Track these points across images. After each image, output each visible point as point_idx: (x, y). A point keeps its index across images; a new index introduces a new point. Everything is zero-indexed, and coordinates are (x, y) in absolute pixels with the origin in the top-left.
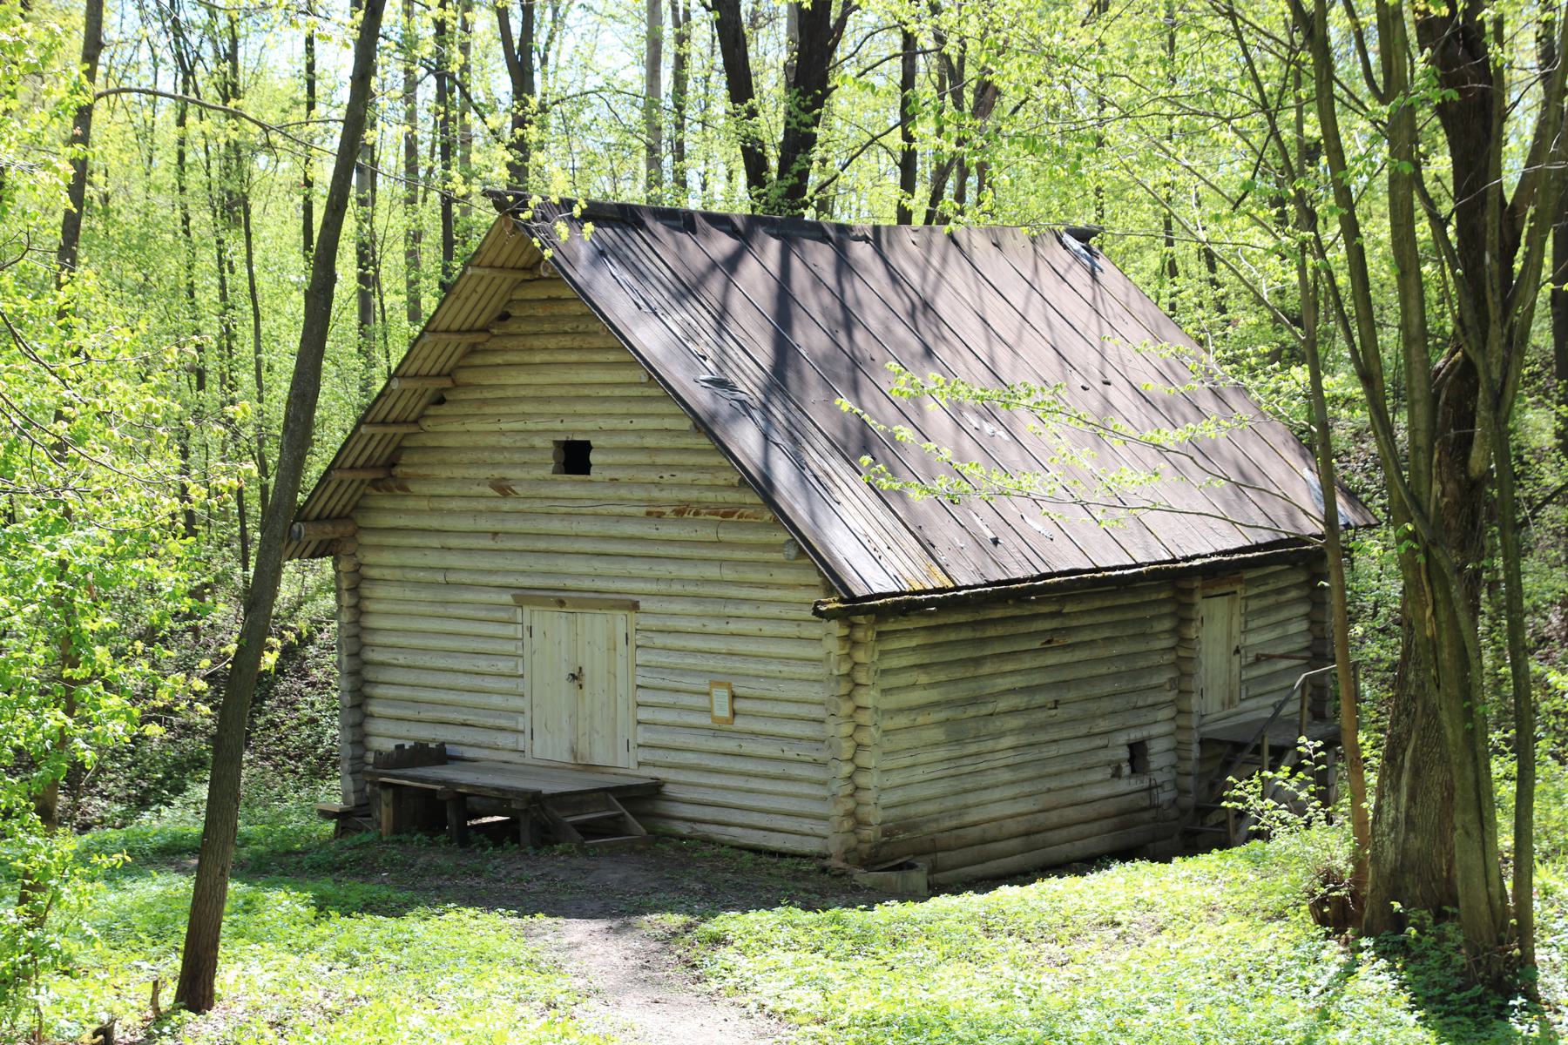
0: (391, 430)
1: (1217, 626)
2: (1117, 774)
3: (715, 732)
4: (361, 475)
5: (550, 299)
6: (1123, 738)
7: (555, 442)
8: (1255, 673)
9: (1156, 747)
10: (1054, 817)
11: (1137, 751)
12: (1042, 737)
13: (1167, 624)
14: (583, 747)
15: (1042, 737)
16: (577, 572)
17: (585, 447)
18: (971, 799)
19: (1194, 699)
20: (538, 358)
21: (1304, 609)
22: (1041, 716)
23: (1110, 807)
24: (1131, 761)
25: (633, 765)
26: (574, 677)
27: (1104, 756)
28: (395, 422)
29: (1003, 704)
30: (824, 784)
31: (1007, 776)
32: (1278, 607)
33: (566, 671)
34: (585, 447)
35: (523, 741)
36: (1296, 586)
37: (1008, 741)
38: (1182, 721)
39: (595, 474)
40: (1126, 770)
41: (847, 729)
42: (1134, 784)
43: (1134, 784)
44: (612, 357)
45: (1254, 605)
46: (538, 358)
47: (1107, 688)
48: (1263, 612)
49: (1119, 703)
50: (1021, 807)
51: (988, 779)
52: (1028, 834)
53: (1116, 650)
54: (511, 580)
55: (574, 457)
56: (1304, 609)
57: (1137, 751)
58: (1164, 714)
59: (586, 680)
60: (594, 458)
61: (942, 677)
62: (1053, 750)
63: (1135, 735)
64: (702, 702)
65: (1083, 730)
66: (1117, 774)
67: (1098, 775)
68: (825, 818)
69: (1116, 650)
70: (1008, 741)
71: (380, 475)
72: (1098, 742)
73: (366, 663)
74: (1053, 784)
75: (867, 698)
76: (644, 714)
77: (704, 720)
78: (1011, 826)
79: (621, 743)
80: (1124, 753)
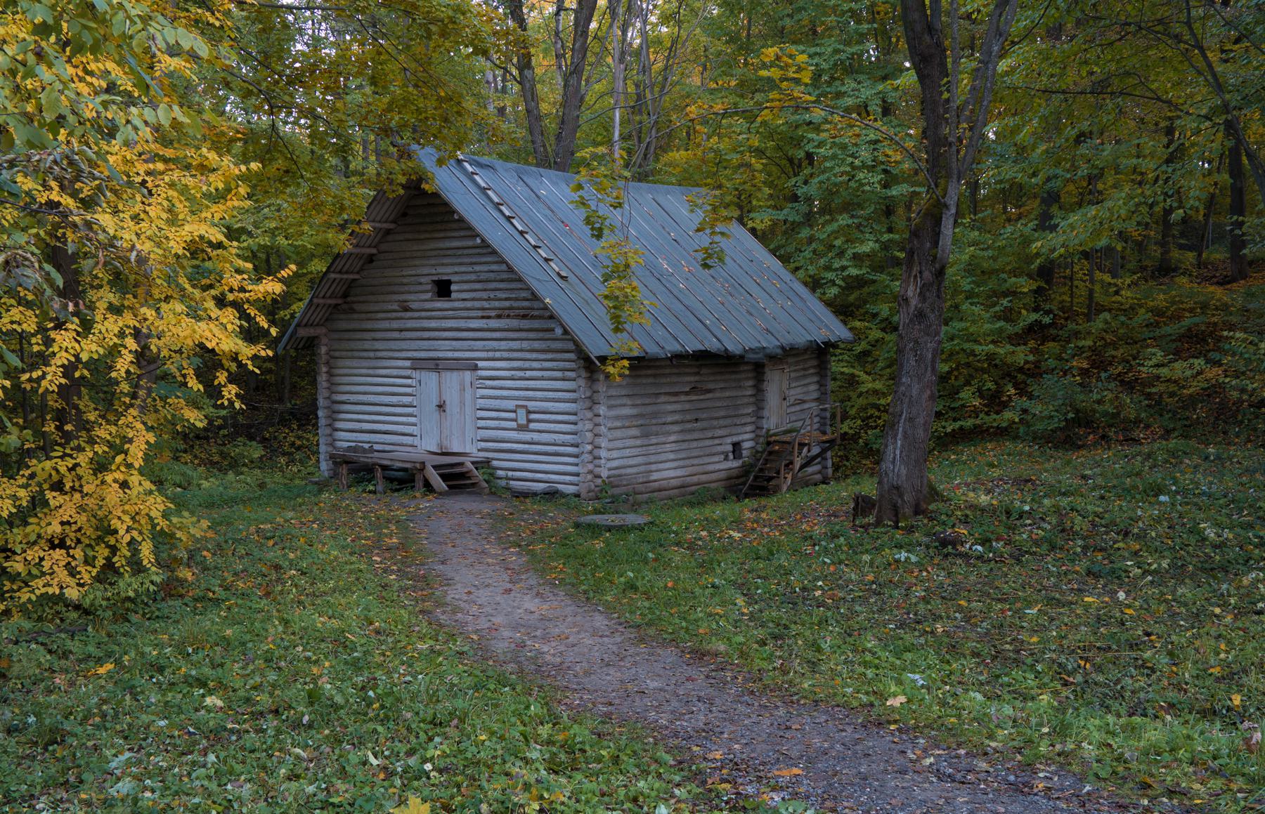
0: (345, 276)
1: (776, 384)
2: (726, 459)
3: (521, 428)
4: (329, 301)
5: (429, 205)
6: (729, 440)
7: (434, 281)
8: (793, 409)
9: (746, 445)
10: (695, 479)
11: (736, 446)
12: (689, 437)
13: (751, 383)
14: (445, 443)
15: (689, 437)
16: (445, 350)
17: (449, 283)
18: (654, 467)
19: (764, 421)
20: (422, 236)
21: (815, 379)
22: (689, 426)
23: (723, 475)
24: (734, 452)
25: (475, 451)
26: (440, 406)
27: (719, 449)
28: (347, 272)
29: (669, 419)
30: (576, 456)
31: (672, 456)
32: (805, 376)
33: (436, 402)
34: (449, 283)
35: (416, 441)
36: (814, 367)
37: (672, 438)
38: (758, 432)
39: (454, 295)
40: (731, 456)
41: (589, 426)
42: (736, 464)
43: (736, 464)
44: (462, 233)
45: (793, 375)
46: (422, 236)
47: (722, 413)
48: (797, 379)
49: (728, 421)
50: (679, 473)
51: (663, 457)
52: (682, 487)
53: (727, 394)
54: (409, 354)
55: (443, 289)
56: (815, 379)
57: (736, 446)
58: (749, 428)
59: (448, 408)
60: (453, 287)
61: (639, 402)
62: (695, 444)
63: (735, 439)
64: (512, 415)
65: (710, 435)
66: (726, 459)
67: (716, 459)
68: (577, 475)
69: (727, 394)
70: (672, 438)
71: (339, 301)
72: (717, 441)
73: (337, 430)
74: (696, 461)
75: (602, 410)
76: (481, 423)
77: (514, 424)
78: (674, 483)
79: (468, 439)
80: (730, 448)
